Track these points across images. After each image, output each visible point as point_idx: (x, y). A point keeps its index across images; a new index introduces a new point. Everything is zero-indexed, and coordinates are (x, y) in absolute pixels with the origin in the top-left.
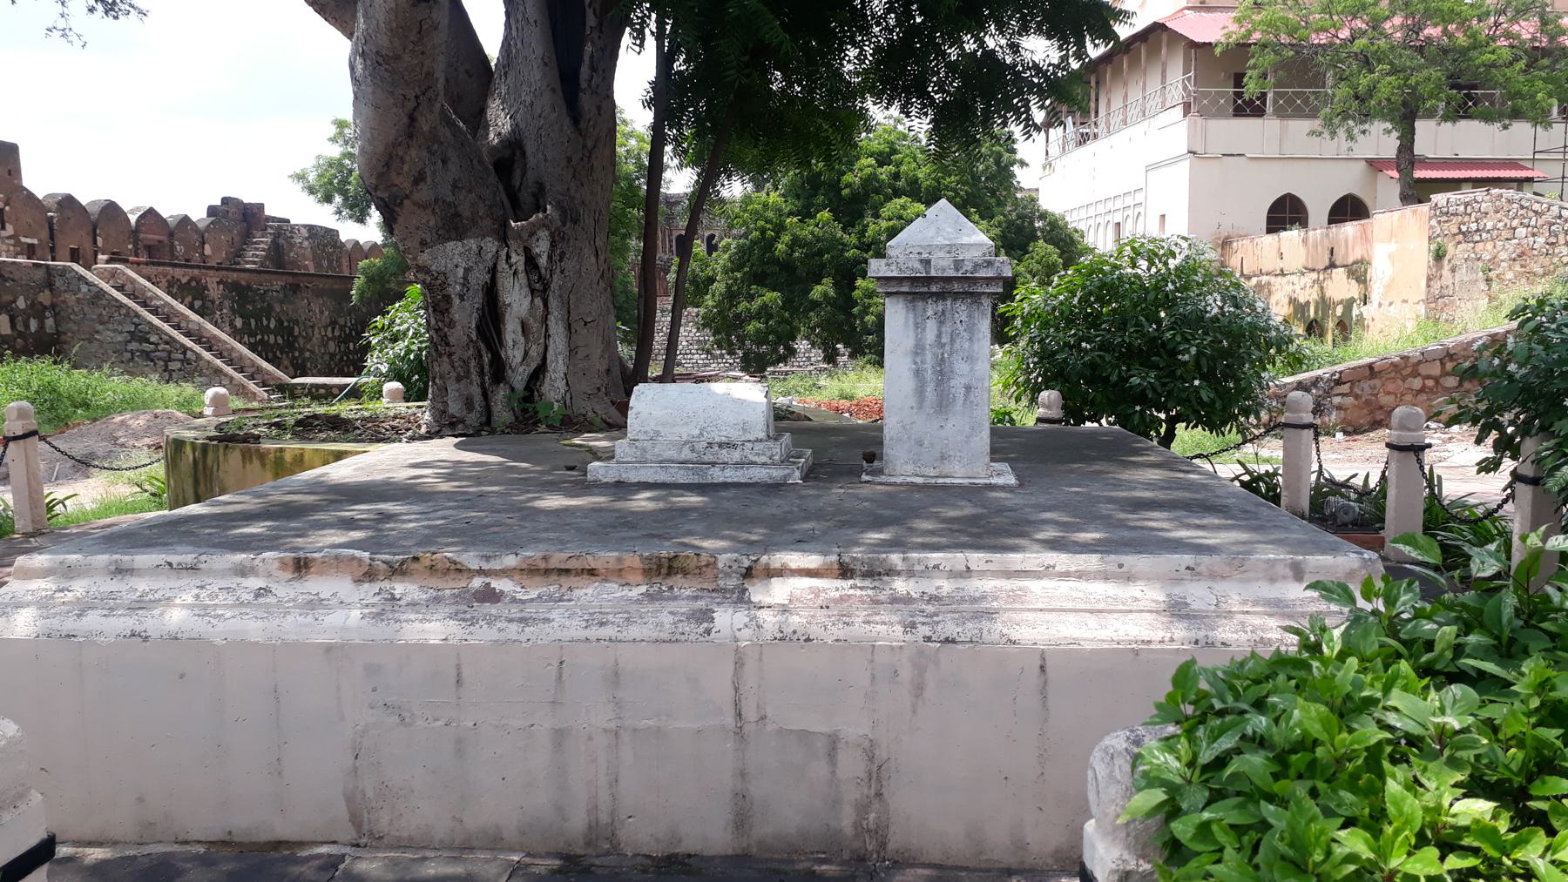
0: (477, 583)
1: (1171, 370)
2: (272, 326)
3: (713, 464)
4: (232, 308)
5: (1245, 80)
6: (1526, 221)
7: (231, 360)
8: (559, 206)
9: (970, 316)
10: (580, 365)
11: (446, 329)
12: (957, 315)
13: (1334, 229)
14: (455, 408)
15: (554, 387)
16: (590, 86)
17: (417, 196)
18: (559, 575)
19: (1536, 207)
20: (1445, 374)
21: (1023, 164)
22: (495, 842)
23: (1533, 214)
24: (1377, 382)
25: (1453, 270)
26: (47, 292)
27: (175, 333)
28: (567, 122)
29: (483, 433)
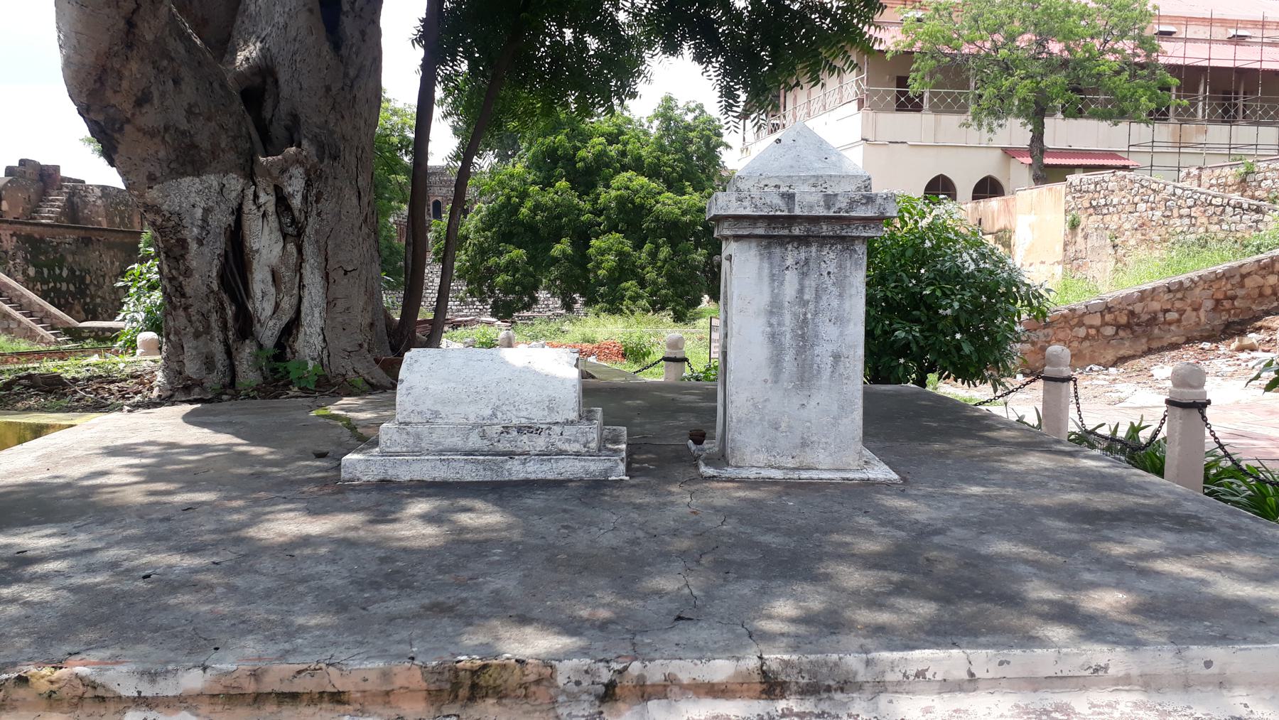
1: (932, 324)
2: (64, 274)
3: (511, 455)
4: (25, 259)
5: (909, 81)
6: (1146, 197)
7: (21, 305)
8: (315, 140)
9: (840, 266)
10: (340, 320)
11: (181, 278)
12: (823, 265)
13: (982, 204)
14: (192, 368)
15: (309, 343)
16: (353, 9)
18: (280, 704)
19: (1154, 186)
20: (1105, 324)
21: (728, 146)
23: (1151, 192)
24: (1050, 331)
25: (1086, 237)
28: (326, 48)
29: (225, 397)
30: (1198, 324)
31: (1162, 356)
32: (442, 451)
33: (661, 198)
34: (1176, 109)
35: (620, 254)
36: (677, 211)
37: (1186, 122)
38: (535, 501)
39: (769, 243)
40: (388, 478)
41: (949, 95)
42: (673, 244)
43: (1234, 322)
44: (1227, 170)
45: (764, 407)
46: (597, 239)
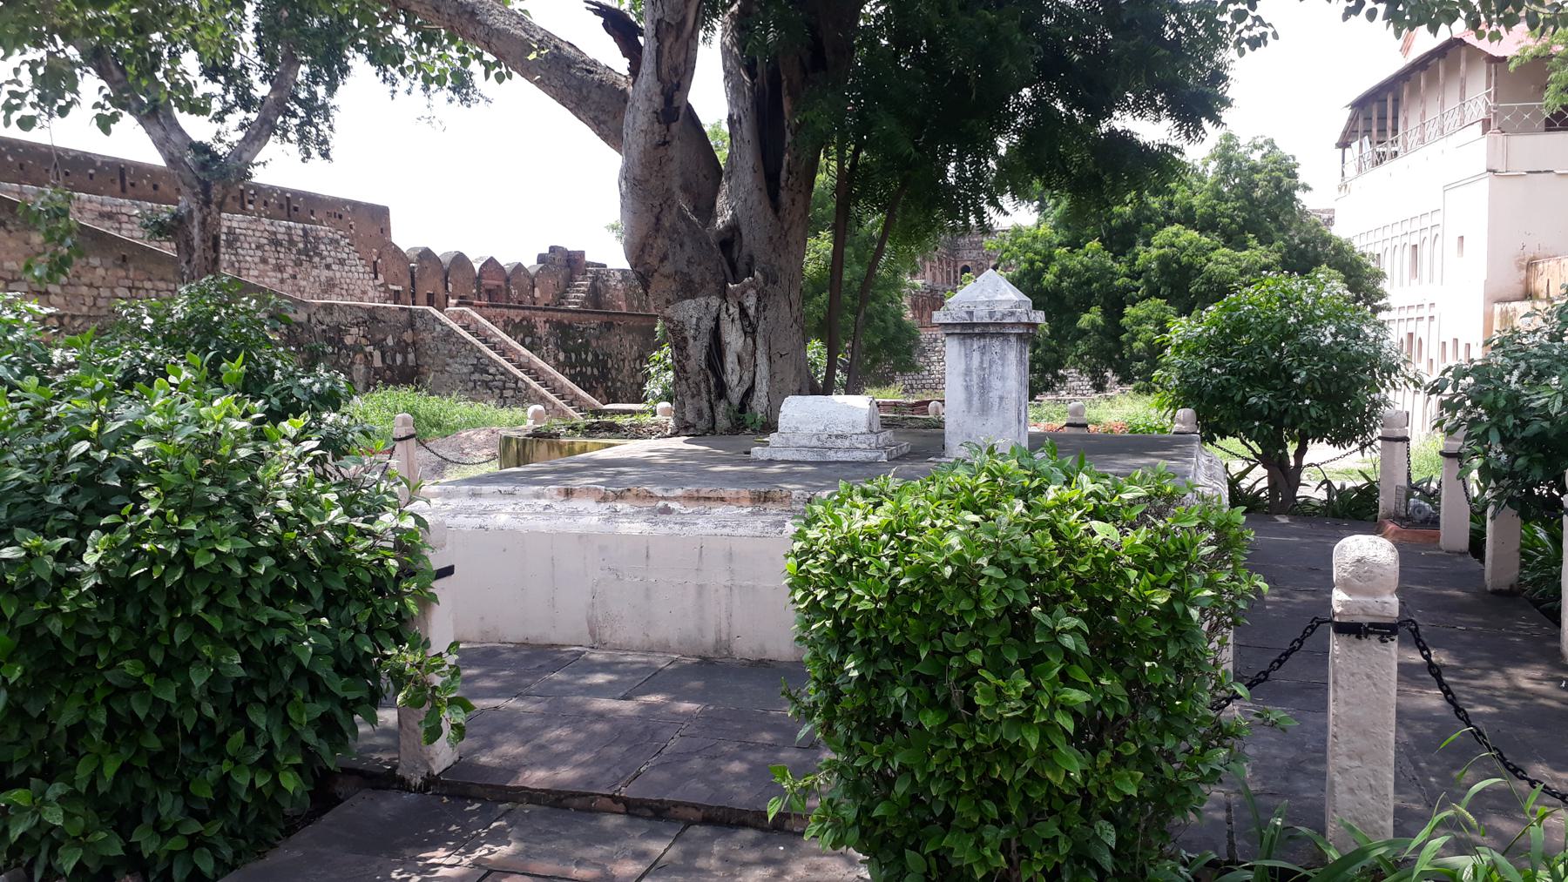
0: (661, 504)
3: (830, 449)
4: (556, 344)
8: (762, 271)
9: (1002, 349)
17: (662, 270)
21: (1306, 188)
22: (665, 649)
26: (410, 331)
27: (509, 366)
28: (770, 212)
33: (1213, 255)
36: (1233, 270)
46: (1134, 306)
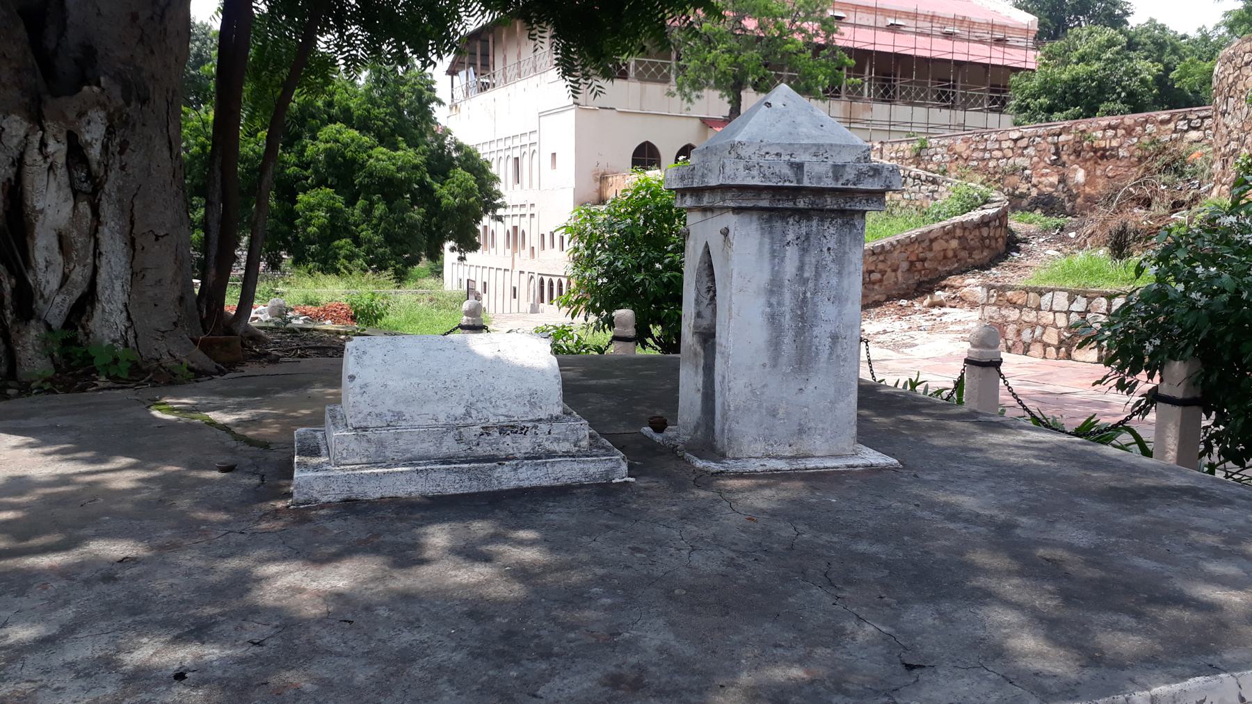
9: (840, 242)
30: (896, 283)
31: (869, 312)
32: (410, 459)
33: (375, 152)
34: (847, 88)
35: (332, 210)
36: (392, 167)
37: (855, 100)
38: (557, 514)
39: (770, 216)
40: (354, 497)
41: (653, 64)
42: (388, 199)
43: (924, 282)
44: (904, 145)
45: (762, 393)
46: (305, 193)
